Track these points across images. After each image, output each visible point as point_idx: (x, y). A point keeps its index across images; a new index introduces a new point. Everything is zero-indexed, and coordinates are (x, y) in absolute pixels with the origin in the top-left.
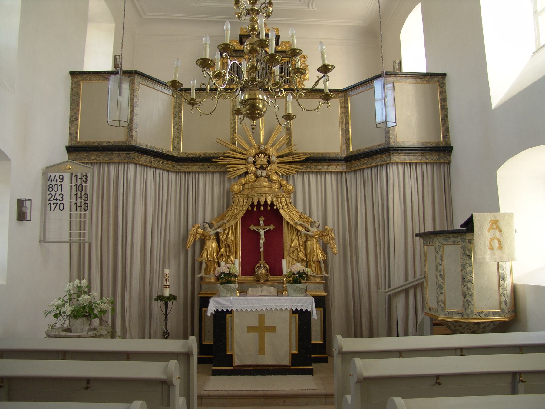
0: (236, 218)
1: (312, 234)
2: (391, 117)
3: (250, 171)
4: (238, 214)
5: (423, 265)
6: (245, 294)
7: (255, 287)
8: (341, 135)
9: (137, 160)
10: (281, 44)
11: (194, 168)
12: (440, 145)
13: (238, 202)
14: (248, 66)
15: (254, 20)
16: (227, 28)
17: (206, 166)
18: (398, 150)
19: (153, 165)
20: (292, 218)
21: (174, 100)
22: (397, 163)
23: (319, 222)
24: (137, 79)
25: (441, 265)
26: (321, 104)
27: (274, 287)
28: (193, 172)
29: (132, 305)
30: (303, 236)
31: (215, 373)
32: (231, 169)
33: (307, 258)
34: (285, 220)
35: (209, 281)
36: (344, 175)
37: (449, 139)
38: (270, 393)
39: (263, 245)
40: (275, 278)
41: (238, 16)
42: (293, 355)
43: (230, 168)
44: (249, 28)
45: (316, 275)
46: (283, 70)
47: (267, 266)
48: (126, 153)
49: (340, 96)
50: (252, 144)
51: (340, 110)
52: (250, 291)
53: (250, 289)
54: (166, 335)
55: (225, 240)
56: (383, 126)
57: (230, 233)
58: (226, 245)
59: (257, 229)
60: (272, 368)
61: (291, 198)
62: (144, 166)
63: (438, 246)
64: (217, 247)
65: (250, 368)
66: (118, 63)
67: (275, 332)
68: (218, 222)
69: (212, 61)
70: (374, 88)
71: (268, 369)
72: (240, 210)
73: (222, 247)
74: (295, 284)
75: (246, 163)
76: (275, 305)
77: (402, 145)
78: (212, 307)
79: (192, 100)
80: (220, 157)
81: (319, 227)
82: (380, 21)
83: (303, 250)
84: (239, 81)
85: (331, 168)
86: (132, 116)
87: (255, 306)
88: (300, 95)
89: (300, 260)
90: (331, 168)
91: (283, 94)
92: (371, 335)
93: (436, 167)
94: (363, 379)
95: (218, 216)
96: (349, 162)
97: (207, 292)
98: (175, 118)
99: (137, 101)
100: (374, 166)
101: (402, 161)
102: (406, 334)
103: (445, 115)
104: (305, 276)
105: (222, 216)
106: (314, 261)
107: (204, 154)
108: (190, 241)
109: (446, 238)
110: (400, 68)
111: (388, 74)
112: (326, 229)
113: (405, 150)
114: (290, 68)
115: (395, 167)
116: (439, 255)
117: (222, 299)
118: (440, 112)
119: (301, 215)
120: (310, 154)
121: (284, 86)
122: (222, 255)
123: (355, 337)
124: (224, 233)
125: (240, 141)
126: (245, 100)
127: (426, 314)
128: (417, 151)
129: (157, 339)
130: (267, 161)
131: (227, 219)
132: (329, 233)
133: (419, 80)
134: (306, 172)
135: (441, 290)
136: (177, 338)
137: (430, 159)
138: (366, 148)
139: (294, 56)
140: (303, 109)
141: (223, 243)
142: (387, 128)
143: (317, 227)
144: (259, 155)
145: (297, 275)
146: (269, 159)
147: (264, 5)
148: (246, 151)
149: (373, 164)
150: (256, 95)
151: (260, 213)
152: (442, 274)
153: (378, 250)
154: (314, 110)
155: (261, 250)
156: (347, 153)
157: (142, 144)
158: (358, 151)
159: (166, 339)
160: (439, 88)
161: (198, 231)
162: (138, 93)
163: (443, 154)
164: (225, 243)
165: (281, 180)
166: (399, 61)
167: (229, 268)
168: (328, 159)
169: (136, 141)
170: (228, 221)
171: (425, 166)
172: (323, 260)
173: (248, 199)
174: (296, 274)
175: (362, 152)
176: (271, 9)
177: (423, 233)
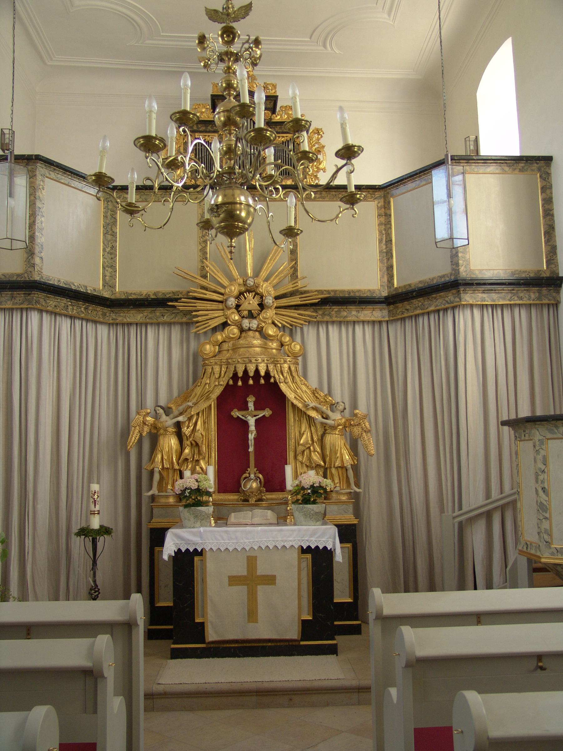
0: (208, 398)
1: (333, 422)
2: (460, 231)
3: (230, 321)
4: (211, 392)
5: (515, 471)
6: (224, 523)
7: (240, 511)
8: (379, 260)
9: (42, 305)
10: (279, 111)
11: (139, 317)
12: (541, 276)
13: (211, 372)
14: (222, 148)
15: (231, 71)
16: (186, 85)
17: (158, 314)
18: (472, 284)
19: (70, 313)
21: (104, 204)
22: (472, 306)
23: (344, 403)
24: (41, 169)
25: (543, 471)
26: (343, 210)
27: (273, 511)
28: (137, 324)
29: (37, 546)
30: (319, 426)
31: (176, 654)
32: (200, 319)
33: (325, 462)
34: (289, 400)
36: (384, 326)
37: (557, 266)
38: (266, 686)
39: (253, 441)
41: (204, 63)
42: (304, 622)
43: (197, 316)
44: (222, 85)
45: (341, 490)
46: (284, 155)
47: (261, 476)
48: (24, 294)
49: (377, 196)
51: (378, 220)
52: (233, 518)
53: (233, 515)
54: (95, 592)
55: (191, 435)
56: (448, 244)
57: (199, 423)
58: (193, 442)
59: (242, 416)
60: (270, 644)
62: (56, 314)
63: (539, 440)
64: (179, 447)
65: (233, 645)
66: (7, 141)
67: (275, 584)
68: (179, 406)
69: (162, 140)
70: (431, 182)
71: (263, 647)
74: (306, 506)
75: (225, 308)
76: (273, 541)
77: (480, 276)
79: (130, 204)
80: (180, 299)
81: (345, 411)
82: (443, 70)
83: (318, 449)
84: (208, 173)
85: (362, 315)
86: (32, 232)
87: (241, 543)
88: (308, 198)
89: (314, 465)
90: (362, 315)
91: (281, 195)
92: (432, 588)
93: (535, 312)
94: (416, 660)
95: (179, 396)
96: (393, 304)
97: (163, 521)
98: (106, 235)
99: (40, 206)
100: (434, 311)
101: (479, 303)
102: (489, 586)
103: (550, 225)
104: (322, 491)
105: (185, 395)
106: (337, 468)
107: (155, 294)
108: (134, 438)
109: (552, 428)
110: (476, 149)
111: (455, 160)
112: (356, 415)
113: (485, 284)
114: (290, 151)
115: (468, 312)
116: (540, 456)
118: (542, 221)
119: (314, 392)
120: (328, 292)
121: (282, 182)
122: (186, 460)
123: (407, 591)
124: (189, 423)
125: (213, 272)
126: (217, 205)
127: (521, 552)
128: (503, 286)
129: (81, 600)
130: (258, 304)
131: (194, 400)
132: (360, 421)
133: (507, 169)
134: (322, 322)
135: (544, 514)
136: (114, 597)
137: (525, 299)
138: (420, 282)
139: (298, 131)
140: (312, 219)
141: (187, 440)
142: (453, 248)
145: (309, 491)
146: (262, 301)
147: (246, 46)
149: (432, 308)
150: (236, 196)
151: (247, 390)
152: (546, 487)
153: (441, 448)
154: (332, 220)
155: (250, 450)
156: (389, 290)
157: (51, 278)
158: (407, 287)
159: (95, 599)
160: (540, 181)
161: (146, 420)
162: (42, 193)
163: (546, 290)
164: (191, 439)
166: (474, 137)
167: (197, 481)
169: (40, 273)
170: (195, 404)
171: (516, 311)
172: (351, 465)
173: (227, 368)
174: (308, 489)
175: (413, 288)
176: (259, 52)
177: (514, 420)
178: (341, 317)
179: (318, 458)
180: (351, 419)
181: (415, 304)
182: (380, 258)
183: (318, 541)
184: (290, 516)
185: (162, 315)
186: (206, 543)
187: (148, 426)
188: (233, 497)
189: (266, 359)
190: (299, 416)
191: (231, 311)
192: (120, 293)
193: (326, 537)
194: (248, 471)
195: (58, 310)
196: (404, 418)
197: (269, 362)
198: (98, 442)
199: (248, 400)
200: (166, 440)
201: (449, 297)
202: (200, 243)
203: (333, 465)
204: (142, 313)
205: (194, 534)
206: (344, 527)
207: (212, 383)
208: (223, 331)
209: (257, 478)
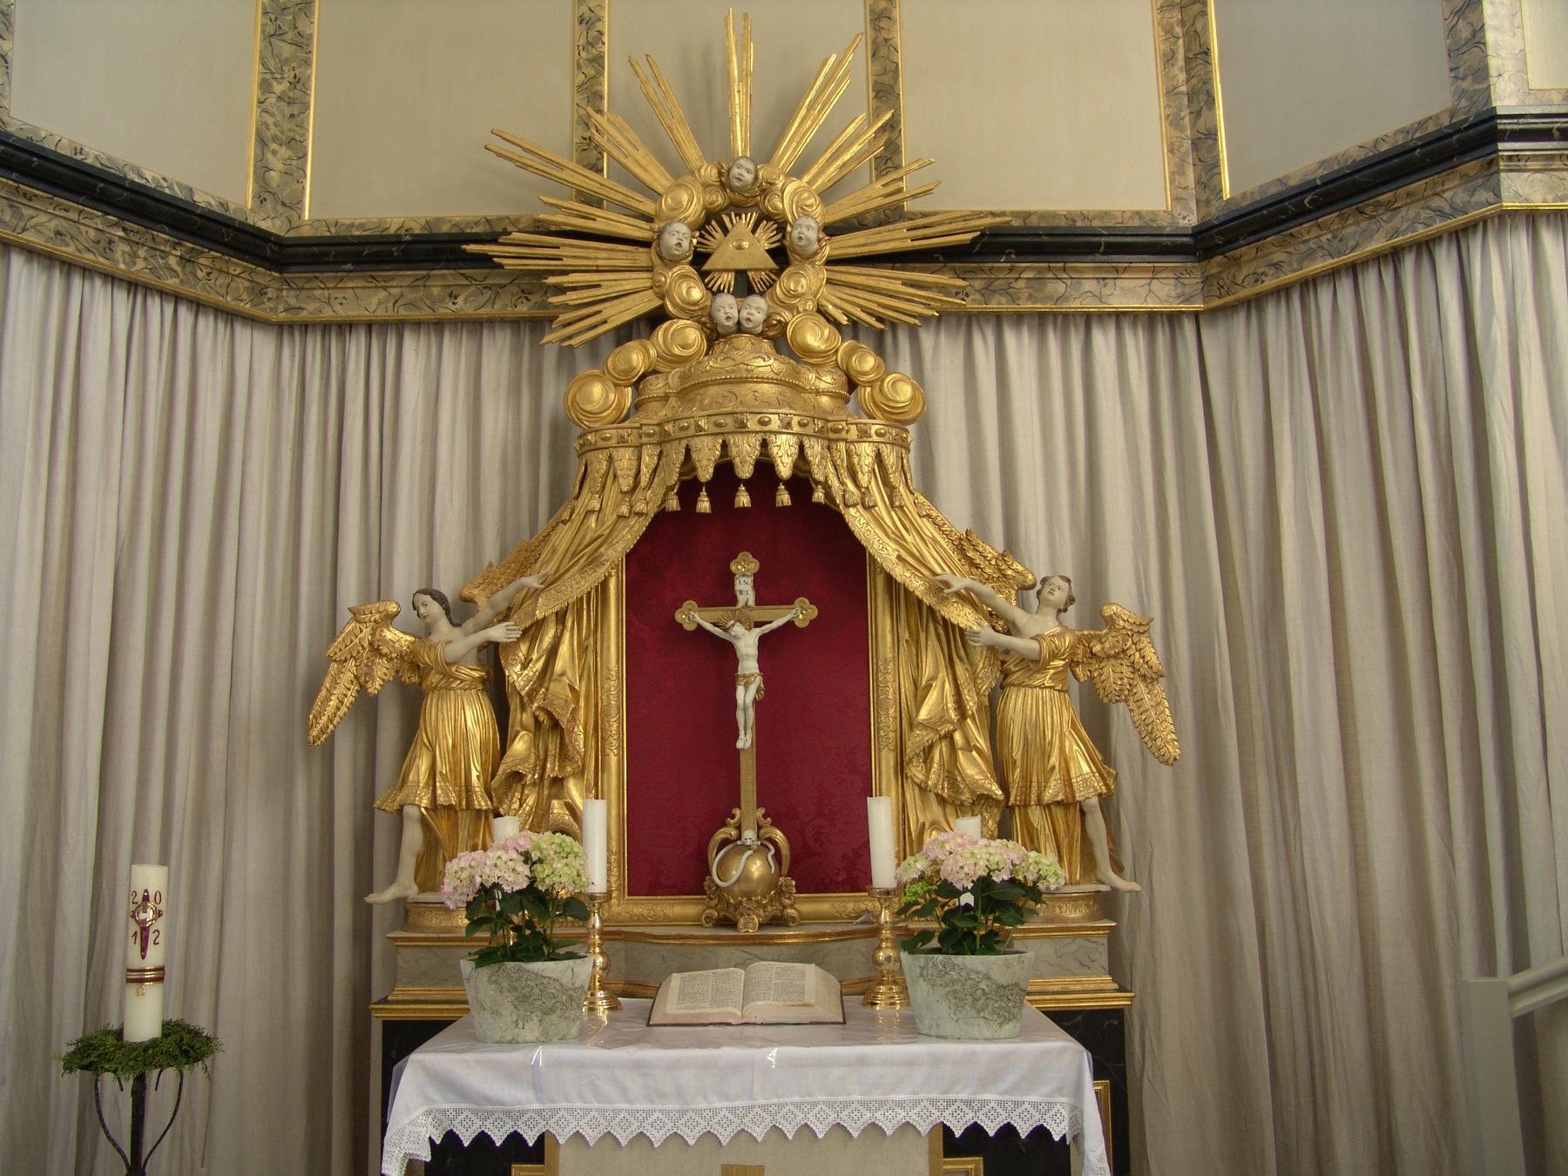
0: (594, 561)
1: (1035, 645)
3: (674, 304)
4: (606, 539)
11: (375, 301)
17: (436, 291)
19: (122, 266)
20: (913, 556)
22: (1532, 218)
32: (571, 298)
35: (443, 930)
36: (1188, 328)
39: (751, 713)
40: (825, 904)
43: (561, 290)
47: (779, 836)
50: (684, 160)
52: (675, 998)
57: (564, 649)
58: (542, 717)
59: (715, 625)
61: (908, 450)
62: (68, 266)
64: (492, 732)
72: (620, 517)
73: (517, 728)
74: (959, 959)
75: (657, 261)
76: (830, 1104)
78: (416, 1114)
83: (982, 742)
85: (1117, 292)
87: (698, 1112)
89: (966, 797)
90: (1117, 292)
100: (1378, 258)
105: (523, 560)
106: (1048, 806)
115: (1519, 244)
117: (478, 1062)
119: (962, 546)
122: (517, 776)
124: (530, 650)
130: (769, 251)
131: (550, 568)
143: (1059, 611)
144: (726, 219)
148: (655, 201)
155: (740, 744)
157: (43, 134)
165: (850, 353)
167: (527, 858)
168: (1103, 239)
172: (1100, 795)
178: (1044, 299)
179: (982, 772)
180: (1091, 637)
181: (1305, 242)
182: (1169, 111)
183: (1010, 1106)
184: (888, 983)
185: (450, 296)
186: (555, 1111)
187: (390, 660)
188: (680, 908)
189: (795, 420)
190: (912, 623)
191: (677, 270)
192: (316, 224)
193: (1044, 1090)
194: (733, 817)
195: (68, 250)
196: (1267, 638)
197: (809, 430)
198: (231, 716)
199: (733, 568)
200: (449, 707)
201: (1448, 195)
202: (579, 67)
203: (1034, 797)
204: (385, 288)
205: (510, 1074)
206: (1079, 1018)
207: (608, 510)
208: (648, 337)
209: (766, 842)
